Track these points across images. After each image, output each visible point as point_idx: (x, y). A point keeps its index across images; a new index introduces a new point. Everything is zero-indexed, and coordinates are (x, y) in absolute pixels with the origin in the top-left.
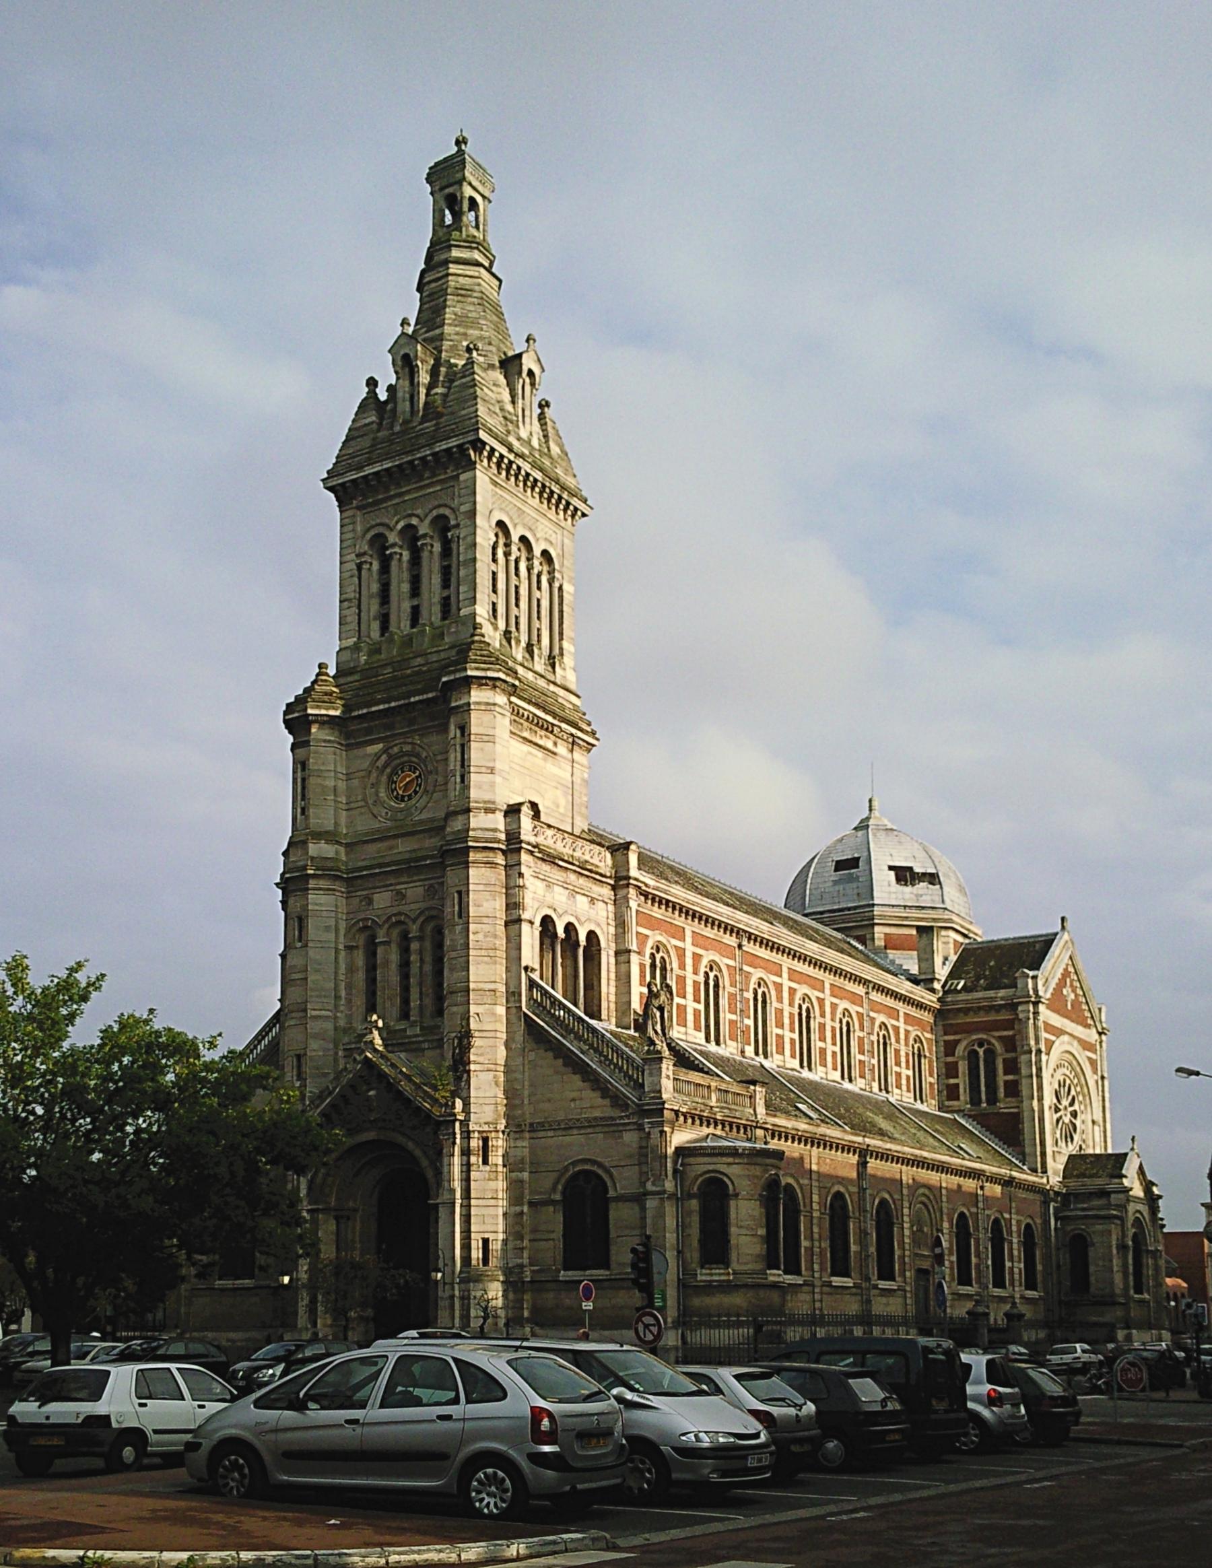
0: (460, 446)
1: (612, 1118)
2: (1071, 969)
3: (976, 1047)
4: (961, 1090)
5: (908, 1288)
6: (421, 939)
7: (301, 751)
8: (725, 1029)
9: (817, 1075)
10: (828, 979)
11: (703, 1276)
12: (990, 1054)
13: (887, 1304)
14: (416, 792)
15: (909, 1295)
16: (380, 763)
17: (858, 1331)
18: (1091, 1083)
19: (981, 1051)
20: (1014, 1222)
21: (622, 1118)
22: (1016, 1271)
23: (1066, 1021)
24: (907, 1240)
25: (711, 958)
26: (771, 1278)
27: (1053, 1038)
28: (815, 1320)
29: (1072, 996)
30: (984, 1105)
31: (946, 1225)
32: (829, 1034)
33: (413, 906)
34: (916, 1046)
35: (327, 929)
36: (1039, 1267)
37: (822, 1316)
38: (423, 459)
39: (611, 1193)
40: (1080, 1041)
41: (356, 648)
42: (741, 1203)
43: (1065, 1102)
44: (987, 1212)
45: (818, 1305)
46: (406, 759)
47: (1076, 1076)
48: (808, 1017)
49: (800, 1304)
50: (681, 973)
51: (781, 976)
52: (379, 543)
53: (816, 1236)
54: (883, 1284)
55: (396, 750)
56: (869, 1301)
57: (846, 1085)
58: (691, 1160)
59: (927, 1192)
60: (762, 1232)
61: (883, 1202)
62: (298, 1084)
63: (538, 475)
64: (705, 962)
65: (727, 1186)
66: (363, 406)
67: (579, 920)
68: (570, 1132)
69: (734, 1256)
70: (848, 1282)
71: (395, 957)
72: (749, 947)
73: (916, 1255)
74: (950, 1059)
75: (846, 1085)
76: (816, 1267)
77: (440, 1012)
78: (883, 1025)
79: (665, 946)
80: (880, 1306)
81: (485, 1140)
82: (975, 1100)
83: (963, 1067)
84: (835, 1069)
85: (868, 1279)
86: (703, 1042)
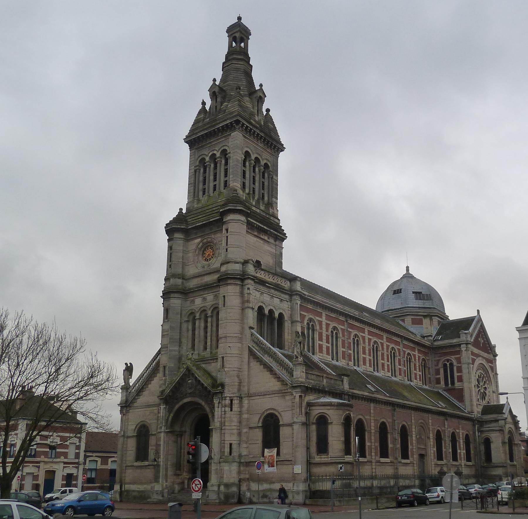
2: (481, 330)
4: (441, 380)
5: (415, 462)
6: (212, 316)
7: (171, 242)
8: (340, 355)
9: (380, 374)
10: (385, 336)
11: (317, 459)
12: (451, 365)
14: (212, 257)
18: (491, 376)
19: (448, 364)
20: (461, 434)
22: (462, 454)
24: (414, 442)
25: (334, 325)
28: (372, 478)
30: (450, 386)
31: (431, 435)
32: (386, 358)
33: (209, 304)
34: (375, 346)
35: (177, 314)
36: (472, 452)
37: (376, 475)
38: (218, 129)
39: (281, 423)
43: (481, 384)
45: (374, 470)
46: (209, 244)
48: (377, 351)
49: (366, 470)
50: (320, 331)
51: (322, 318)
52: (202, 161)
53: (373, 441)
55: (205, 241)
56: (397, 469)
57: (394, 378)
58: (314, 408)
59: (422, 421)
60: (343, 439)
62: (164, 378)
63: (262, 134)
64: (390, 347)
66: (200, 113)
68: (265, 396)
69: (330, 450)
71: (202, 325)
73: (419, 448)
74: (437, 368)
75: (394, 378)
76: (373, 454)
77: (217, 347)
80: (404, 471)
81: (232, 401)
82: (446, 384)
83: (442, 371)
84: (389, 371)
85: (396, 459)
86: (331, 360)
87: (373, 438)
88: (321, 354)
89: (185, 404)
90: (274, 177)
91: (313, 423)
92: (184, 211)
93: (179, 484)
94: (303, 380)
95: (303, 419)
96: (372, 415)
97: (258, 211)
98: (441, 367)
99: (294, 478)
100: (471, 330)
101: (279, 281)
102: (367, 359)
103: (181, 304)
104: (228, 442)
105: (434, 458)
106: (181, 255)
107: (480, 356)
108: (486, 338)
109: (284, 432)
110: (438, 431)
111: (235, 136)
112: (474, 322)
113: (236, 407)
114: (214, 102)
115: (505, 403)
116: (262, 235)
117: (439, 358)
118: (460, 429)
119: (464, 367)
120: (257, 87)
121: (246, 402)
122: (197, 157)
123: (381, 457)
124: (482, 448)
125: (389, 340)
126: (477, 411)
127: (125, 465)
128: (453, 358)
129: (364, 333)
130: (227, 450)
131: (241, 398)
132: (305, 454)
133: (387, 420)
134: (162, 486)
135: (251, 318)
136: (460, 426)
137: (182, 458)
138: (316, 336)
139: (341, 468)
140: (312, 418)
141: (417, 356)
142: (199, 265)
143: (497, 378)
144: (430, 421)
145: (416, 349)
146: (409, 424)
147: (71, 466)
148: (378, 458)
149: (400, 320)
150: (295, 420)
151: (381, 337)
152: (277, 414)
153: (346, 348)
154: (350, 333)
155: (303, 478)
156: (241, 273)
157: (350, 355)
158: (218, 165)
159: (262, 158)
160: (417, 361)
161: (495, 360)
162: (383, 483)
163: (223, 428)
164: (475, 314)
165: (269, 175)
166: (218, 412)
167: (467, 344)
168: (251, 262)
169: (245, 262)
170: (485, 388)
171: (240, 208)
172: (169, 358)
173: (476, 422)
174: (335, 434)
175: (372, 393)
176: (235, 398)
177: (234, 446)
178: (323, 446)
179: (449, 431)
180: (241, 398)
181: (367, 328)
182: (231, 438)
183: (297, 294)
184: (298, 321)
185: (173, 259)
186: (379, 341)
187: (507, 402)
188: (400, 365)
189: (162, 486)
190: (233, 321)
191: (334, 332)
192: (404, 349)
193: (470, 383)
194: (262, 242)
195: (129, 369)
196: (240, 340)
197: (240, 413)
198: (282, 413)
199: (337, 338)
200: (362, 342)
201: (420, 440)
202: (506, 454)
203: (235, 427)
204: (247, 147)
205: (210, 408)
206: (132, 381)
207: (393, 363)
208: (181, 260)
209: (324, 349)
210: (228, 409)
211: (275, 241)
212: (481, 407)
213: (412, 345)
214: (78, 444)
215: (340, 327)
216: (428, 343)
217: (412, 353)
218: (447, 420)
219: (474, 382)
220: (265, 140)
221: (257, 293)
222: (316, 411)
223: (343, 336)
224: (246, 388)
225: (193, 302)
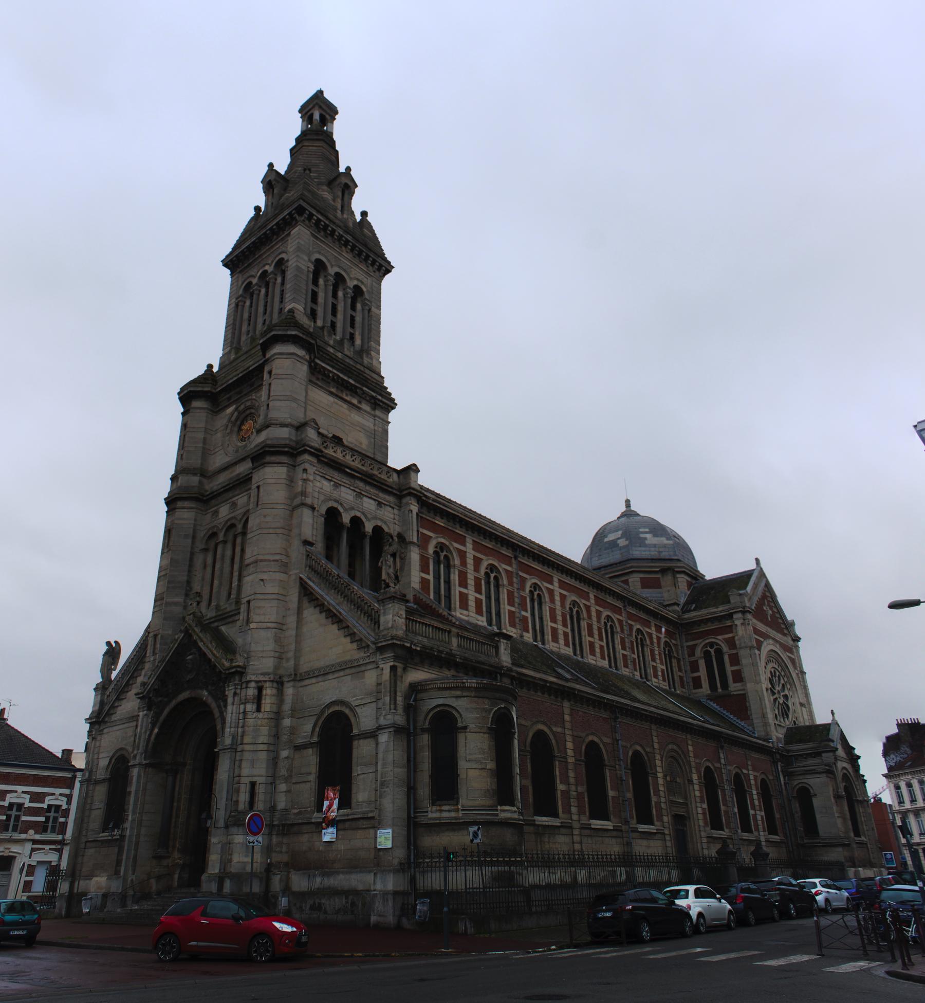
0: (290, 214)
1: (358, 660)
4: (703, 682)
5: (667, 832)
7: (186, 417)
11: (433, 814)
12: (719, 652)
13: (648, 847)
15: (668, 838)
16: (233, 418)
17: (621, 874)
18: (794, 676)
19: (712, 651)
20: (752, 777)
21: (364, 658)
22: (759, 818)
23: (769, 629)
24: (661, 788)
25: (491, 562)
26: (503, 815)
28: (576, 861)
30: (720, 690)
31: (695, 776)
32: (596, 632)
36: (777, 816)
38: (271, 229)
39: (355, 731)
40: (781, 645)
41: (230, 352)
42: (469, 735)
43: (778, 688)
44: (729, 768)
46: (248, 412)
47: (782, 669)
51: (464, 545)
53: (572, 780)
54: (643, 828)
55: (242, 407)
56: (629, 844)
59: (675, 747)
61: (636, 754)
64: (603, 617)
65: (456, 719)
67: (366, 516)
69: (462, 792)
70: (608, 825)
71: (229, 553)
73: (672, 802)
74: (693, 659)
76: (574, 810)
78: (639, 631)
79: (447, 547)
80: (641, 848)
81: (260, 689)
82: (713, 687)
85: (627, 822)
87: (571, 774)
88: (465, 612)
89: (181, 703)
90: (373, 309)
91: (424, 731)
92: (215, 369)
93: (159, 878)
94: (400, 633)
95: (399, 719)
96: (568, 725)
97: (339, 355)
98: (701, 658)
99: (377, 860)
100: (749, 588)
101: (376, 468)
102: (560, 632)
103: (195, 520)
104: (246, 780)
105: (706, 825)
106: (201, 436)
109: (362, 749)
110: (708, 769)
111: (308, 257)
112: (753, 579)
113: (268, 703)
114: (270, 197)
115: (830, 721)
116: (347, 395)
118: (750, 768)
119: (743, 653)
120: (342, 169)
121: (289, 691)
122: (240, 283)
123: (593, 816)
124: (796, 806)
126: (777, 735)
127: (84, 840)
128: (720, 639)
130: (244, 797)
131: (279, 684)
132: (401, 801)
133: (601, 740)
134: (125, 880)
135: (310, 525)
136: (749, 763)
137: (173, 820)
138: (455, 577)
139: (475, 835)
140: (421, 718)
141: (654, 637)
142: (231, 449)
143: (804, 680)
144: (690, 748)
146: (648, 750)
147: (47, 847)
148: (584, 820)
149: (622, 582)
150: (382, 722)
152: (347, 711)
153: (516, 605)
154: (523, 581)
155: (396, 862)
156: (293, 444)
158: (271, 285)
159: (348, 275)
160: (656, 645)
162: (600, 875)
163: (240, 748)
164: (753, 566)
165: (364, 305)
166: (231, 713)
167: (744, 612)
168: (312, 424)
169: (300, 427)
170: (786, 697)
171: (294, 333)
172: (165, 619)
173: (778, 756)
174: (474, 754)
175: (567, 680)
176: (268, 684)
177: (260, 790)
178: (446, 785)
179: (729, 770)
180: (279, 684)
181: (556, 577)
182: (254, 768)
183: (410, 494)
184: (413, 543)
185: (186, 444)
186: (582, 602)
187: (834, 719)
189: (125, 880)
190: (271, 531)
191: (492, 576)
192: (630, 622)
193: (758, 682)
194: (345, 406)
195: (112, 652)
196: (284, 567)
197: (277, 716)
198: (358, 710)
199: (497, 586)
200: (547, 599)
201: (671, 787)
202: (844, 819)
203: (264, 747)
204: (319, 253)
205: (219, 707)
206: (114, 675)
207: (611, 642)
208: (201, 445)
209: (472, 603)
210: (250, 707)
211: (374, 409)
212: (784, 731)
213: (643, 616)
214: (64, 807)
215: (502, 567)
216: (672, 616)
218: (722, 748)
219: (765, 684)
220: (354, 247)
221: (325, 483)
222: (432, 701)
223: (511, 583)
224: (292, 662)
225: (216, 513)
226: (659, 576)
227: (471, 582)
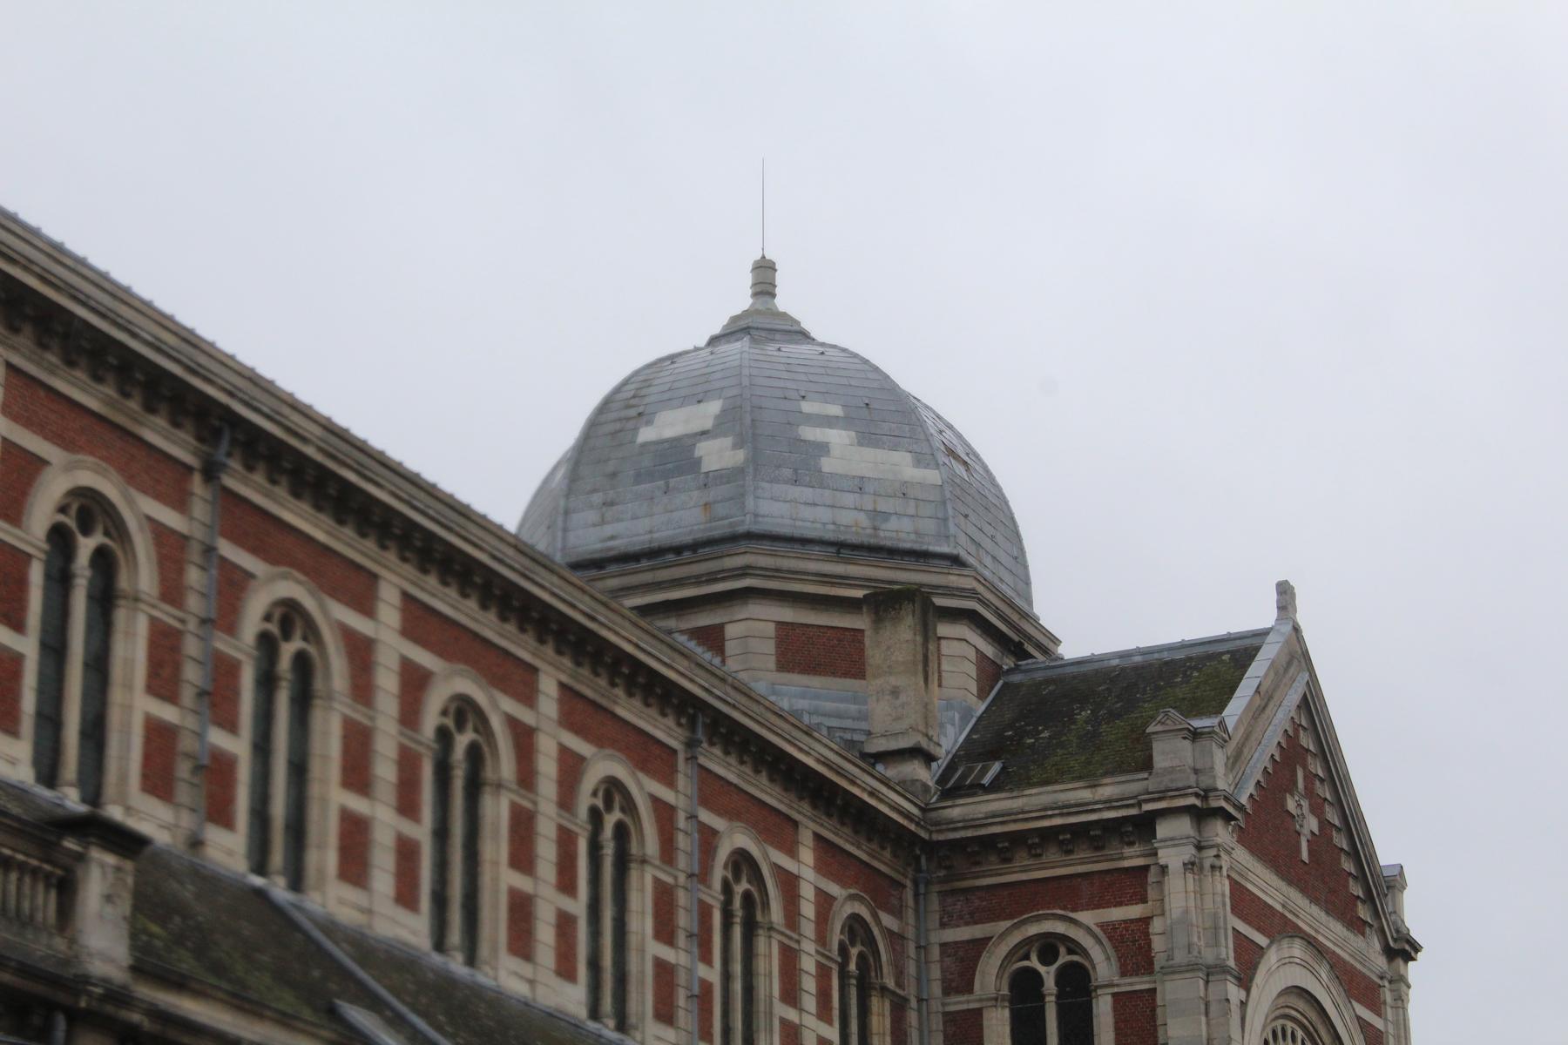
2: (1306, 741)
3: (1034, 962)
12: (1077, 982)
19: (1048, 974)
23: (1296, 896)
25: (87, 479)
27: (1262, 940)
29: (1312, 824)
32: (546, 851)
72: (251, 487)
74: (959, 1003)
78: (742, 862)
100: (1235, 710)
107: (1294, 932)
108: (1339, 804)
112: (1257, 670)
117: (977, 931)
125: (580, 712)
128: (1087, 926)
129: (368, 610)
141: (807, 891)
145: (806, 837)
151: (521, 682)
153: (188, 695)
154: (233, 584)
157: (218, 770)
160: (808, 929)
161: (1400, 981)
181: (395, 580)
186: (499, 706)
188: (665, 932)
191: (86, 546)
192: (706, 817)
215: (141, 509)
216: (892, 804)
217: (770, 857)
223: (172, 592)
226: (860, 622)
227: (385, 771)
